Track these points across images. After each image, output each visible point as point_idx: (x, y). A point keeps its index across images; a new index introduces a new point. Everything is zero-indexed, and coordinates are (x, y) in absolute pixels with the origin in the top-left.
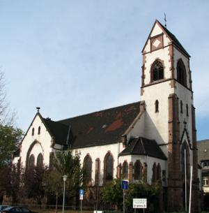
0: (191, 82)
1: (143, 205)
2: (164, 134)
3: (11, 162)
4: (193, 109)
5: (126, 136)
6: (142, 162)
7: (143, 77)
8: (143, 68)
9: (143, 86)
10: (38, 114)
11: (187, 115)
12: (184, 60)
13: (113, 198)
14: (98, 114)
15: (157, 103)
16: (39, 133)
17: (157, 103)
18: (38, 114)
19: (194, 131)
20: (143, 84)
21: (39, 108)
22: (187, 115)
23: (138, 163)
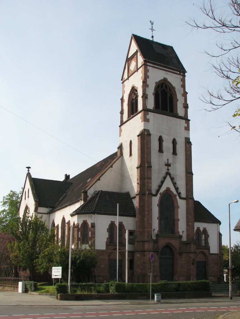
0: (186, 107)
1: (56, 270)
2: (134, 187)
3: (52, 266)
4: (188, 143)
5: (86, 193)
6: (89, 223)
7: (122, 113)
8: (122, 100)
9: (122, 123)
10: (168, 173)
11: (174, 153)
12: (173, 79)
13: (28, 258)
14: (190, 167)
15: (131, 141)
16: (28, 197)
17: (131, 141)
18: (168, 173)
19: (189, 174)
20: (122, 121)
21: (29, 168)
22: (174, 153)
23: (85, 223)
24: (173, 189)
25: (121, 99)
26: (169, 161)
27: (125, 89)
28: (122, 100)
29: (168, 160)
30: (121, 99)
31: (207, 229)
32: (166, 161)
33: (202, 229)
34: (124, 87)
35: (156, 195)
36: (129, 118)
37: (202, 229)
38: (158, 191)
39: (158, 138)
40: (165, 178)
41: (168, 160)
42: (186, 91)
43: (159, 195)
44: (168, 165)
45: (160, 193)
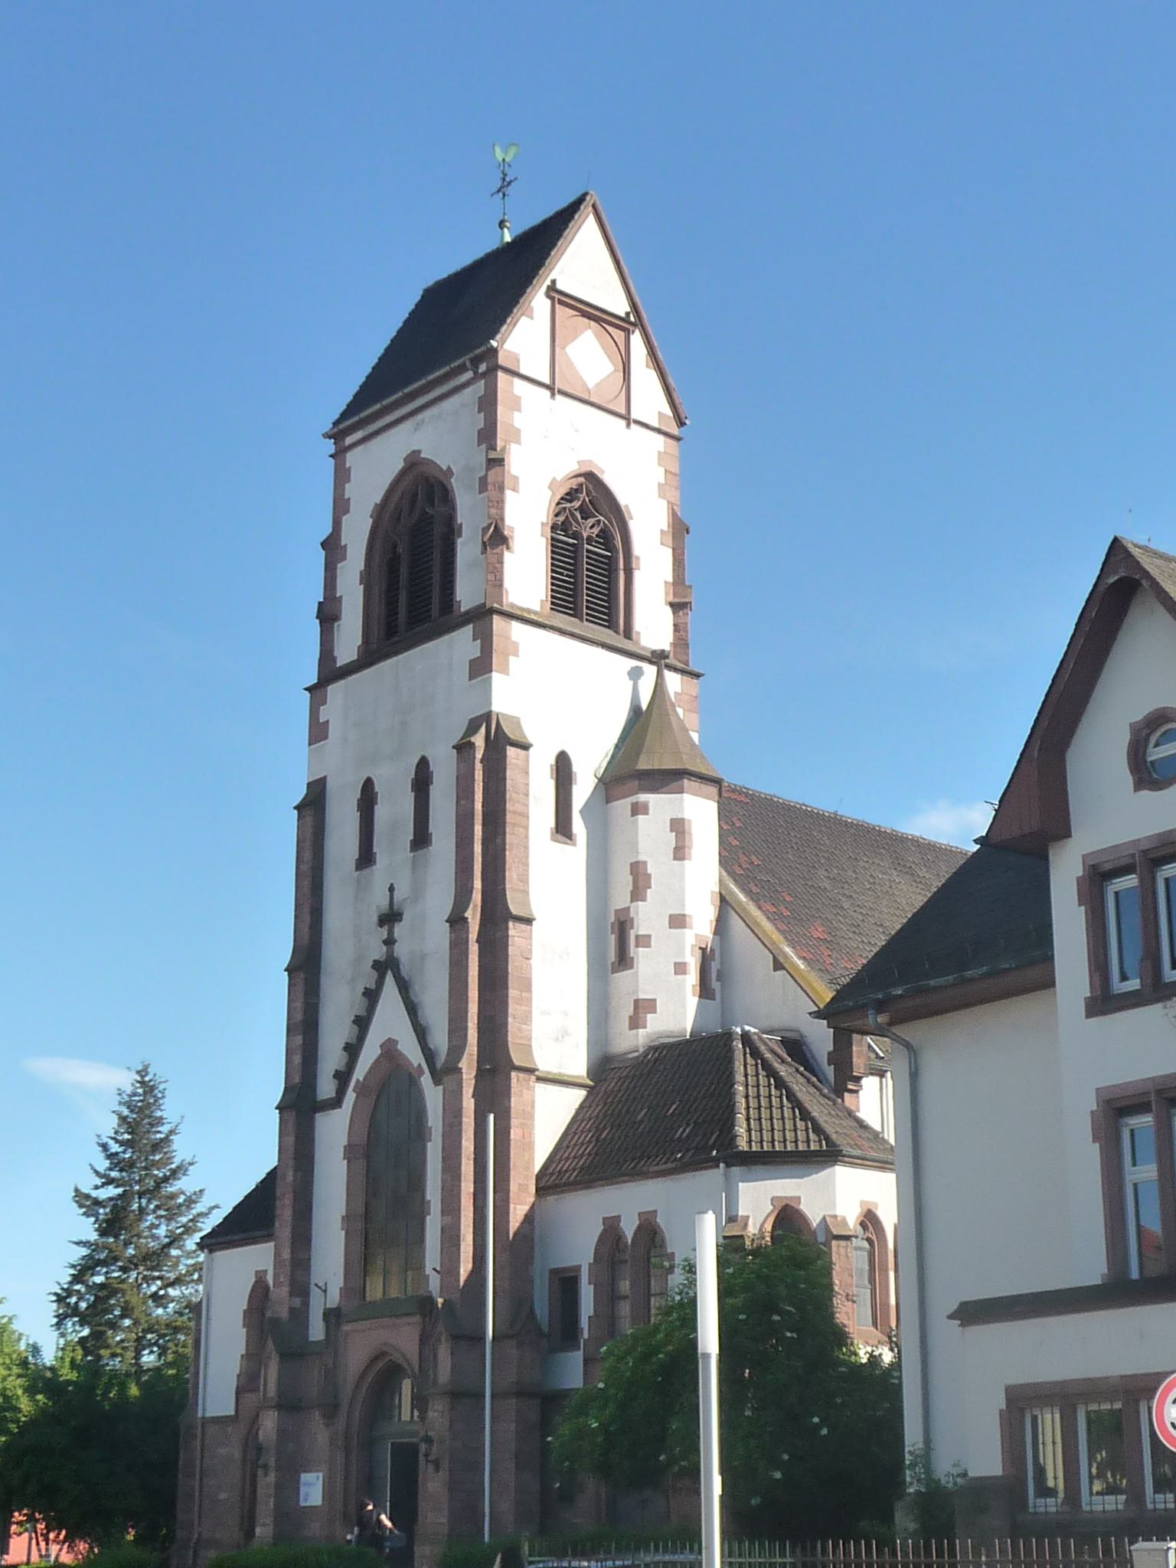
7: (328, 615)
9: (330, 673)
10: (386, 966)
18: (386, 966)
24: (412, 1053)
25: (324, 545)
26: (396, 893)
27: (350, 490)
28: (333, 547)
29: (391, 889)
30: (324, 545)
31: (660, 1220)
32: (384, 903)
33: (629, 1228)
34: (342, 476)
35: (336, 1102)
36: (369, 657)
37: (629, 1228)
38: (343, 1077)
39: (553, 762)
40: (372, 996)
41: (391, 889)
42: (330, 530)
43: (350, 1097)
44: (390, 918)
45: (358, 1080)
